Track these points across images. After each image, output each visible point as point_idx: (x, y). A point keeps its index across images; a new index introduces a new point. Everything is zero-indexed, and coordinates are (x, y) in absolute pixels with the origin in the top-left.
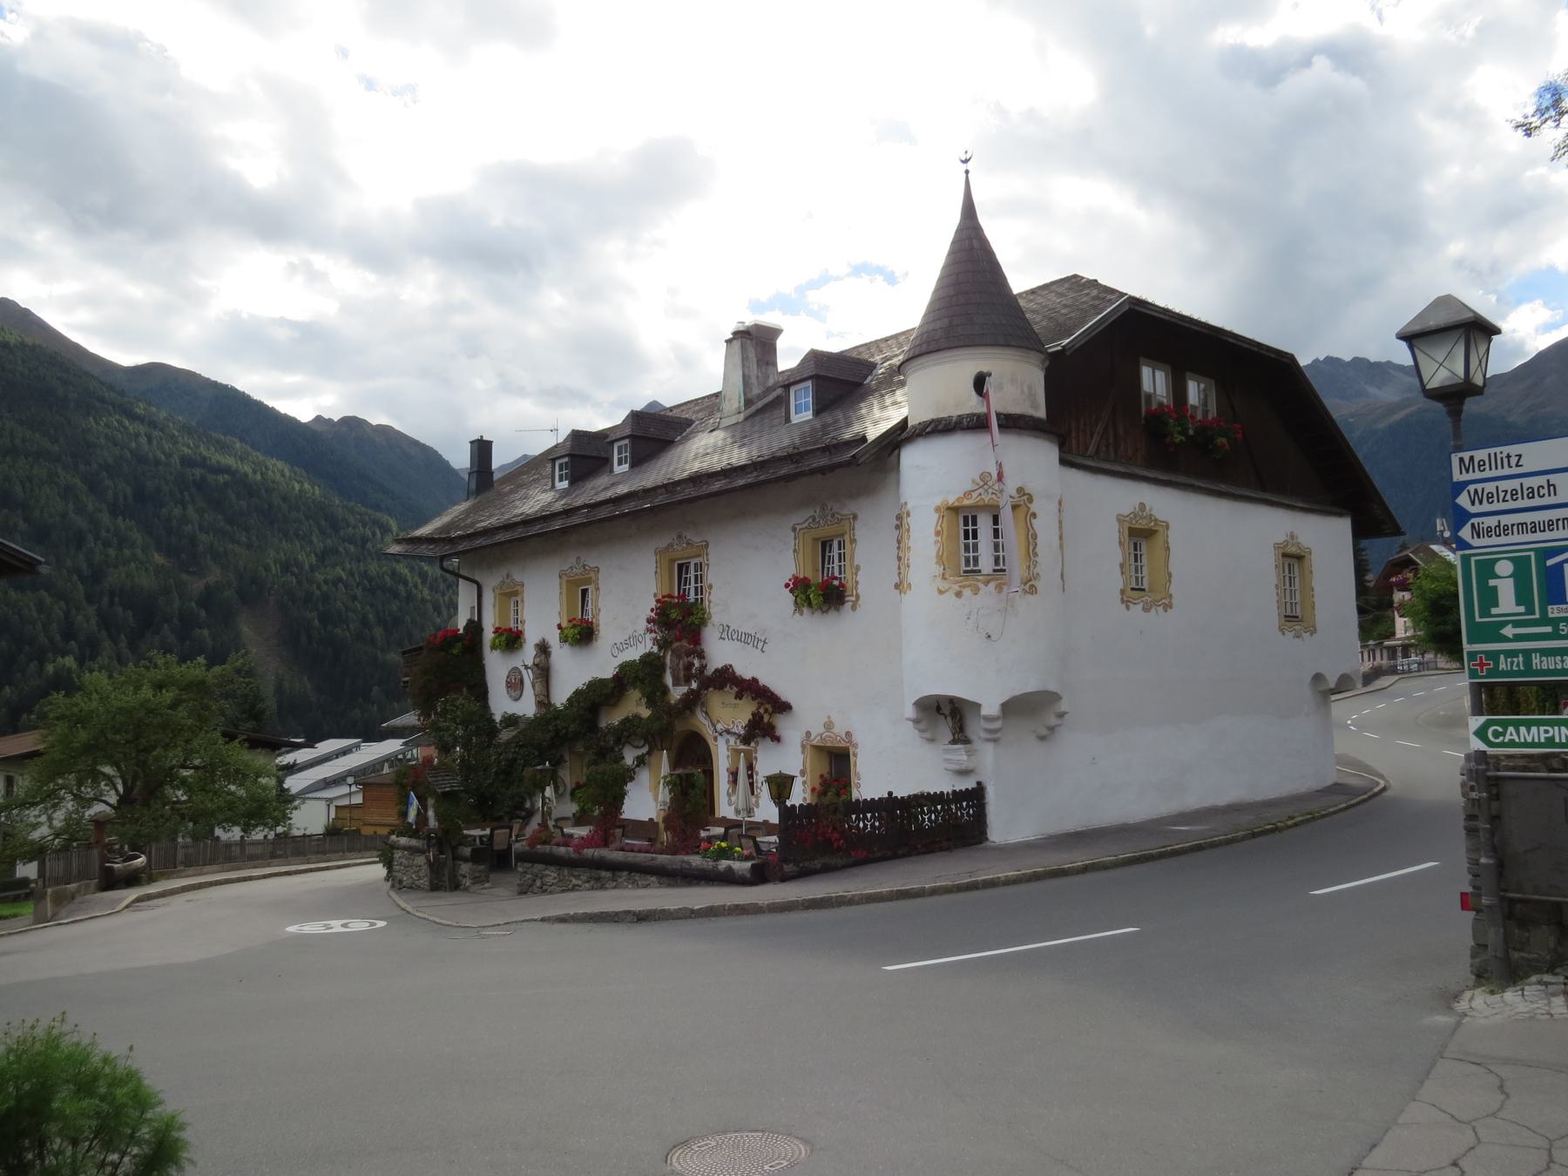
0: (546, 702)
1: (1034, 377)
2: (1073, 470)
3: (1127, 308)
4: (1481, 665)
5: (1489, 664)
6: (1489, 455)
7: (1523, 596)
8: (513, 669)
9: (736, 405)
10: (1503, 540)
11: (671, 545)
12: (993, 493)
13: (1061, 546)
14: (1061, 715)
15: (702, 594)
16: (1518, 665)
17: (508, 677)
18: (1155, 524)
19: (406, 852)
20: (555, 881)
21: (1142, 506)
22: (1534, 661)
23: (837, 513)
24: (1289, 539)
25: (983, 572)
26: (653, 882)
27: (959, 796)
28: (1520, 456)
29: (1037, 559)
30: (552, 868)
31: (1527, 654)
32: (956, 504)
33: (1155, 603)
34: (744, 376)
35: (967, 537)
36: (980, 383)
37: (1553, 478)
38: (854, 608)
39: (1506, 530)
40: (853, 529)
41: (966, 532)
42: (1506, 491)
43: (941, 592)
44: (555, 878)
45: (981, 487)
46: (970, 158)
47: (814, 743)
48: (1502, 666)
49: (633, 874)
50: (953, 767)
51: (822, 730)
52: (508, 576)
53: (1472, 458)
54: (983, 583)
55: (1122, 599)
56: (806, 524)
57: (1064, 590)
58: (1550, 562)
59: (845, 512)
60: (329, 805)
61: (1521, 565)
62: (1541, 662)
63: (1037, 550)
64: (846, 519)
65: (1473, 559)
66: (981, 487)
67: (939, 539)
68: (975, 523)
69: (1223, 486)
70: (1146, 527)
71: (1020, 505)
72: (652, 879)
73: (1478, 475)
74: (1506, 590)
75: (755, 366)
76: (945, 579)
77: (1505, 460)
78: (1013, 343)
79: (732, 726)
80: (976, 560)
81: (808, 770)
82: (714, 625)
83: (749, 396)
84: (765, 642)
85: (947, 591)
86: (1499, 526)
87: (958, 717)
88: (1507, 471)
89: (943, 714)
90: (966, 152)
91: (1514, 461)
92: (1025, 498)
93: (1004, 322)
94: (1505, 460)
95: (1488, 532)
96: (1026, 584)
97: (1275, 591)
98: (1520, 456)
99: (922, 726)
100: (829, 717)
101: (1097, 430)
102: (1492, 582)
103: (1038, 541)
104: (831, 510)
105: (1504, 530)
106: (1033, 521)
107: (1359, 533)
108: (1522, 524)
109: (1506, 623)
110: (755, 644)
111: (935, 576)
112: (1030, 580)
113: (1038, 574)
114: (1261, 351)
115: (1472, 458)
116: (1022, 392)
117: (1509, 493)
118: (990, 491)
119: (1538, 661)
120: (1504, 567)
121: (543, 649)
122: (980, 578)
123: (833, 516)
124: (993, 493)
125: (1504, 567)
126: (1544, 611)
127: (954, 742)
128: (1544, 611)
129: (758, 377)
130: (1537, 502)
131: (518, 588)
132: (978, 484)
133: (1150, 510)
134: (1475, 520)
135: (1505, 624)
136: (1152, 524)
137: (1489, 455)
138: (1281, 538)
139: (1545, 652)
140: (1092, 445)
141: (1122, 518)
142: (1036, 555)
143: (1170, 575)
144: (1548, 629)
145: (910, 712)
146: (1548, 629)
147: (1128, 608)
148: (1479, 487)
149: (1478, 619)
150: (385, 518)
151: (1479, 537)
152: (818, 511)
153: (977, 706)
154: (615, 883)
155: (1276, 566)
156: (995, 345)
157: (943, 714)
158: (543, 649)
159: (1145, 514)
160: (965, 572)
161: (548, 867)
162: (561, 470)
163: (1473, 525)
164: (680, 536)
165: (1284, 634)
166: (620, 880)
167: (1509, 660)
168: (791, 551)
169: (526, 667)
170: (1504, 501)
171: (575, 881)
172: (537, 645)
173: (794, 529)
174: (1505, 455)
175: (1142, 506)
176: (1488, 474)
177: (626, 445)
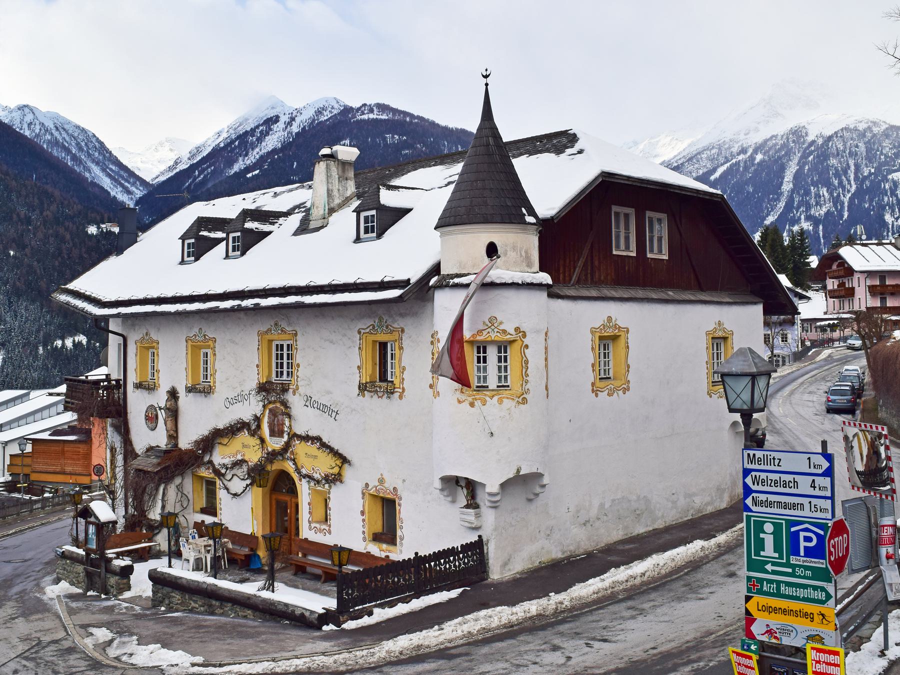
0: (175, 435)
1: (531, 242)
2: (560, 300)
3: (601, 180)
4: (754, 586)
5: (758, 586)
6: (764, 455)
7: (777, 548)
8: (150, 406)
9: (322, 212)
10: (768, 510)
11: (269, 330)
12: (497, 332)
13: (546, 366)
14: (544, 486)
15: (292, 369)
16: (773, 589)
17: (146, 412)
18: (619, 330)
19: (68, 561)
20: (179, 602)
21: (610, 319)
22: (782, 588)
23: (391, 326)
24: (717, 326)
25: (490, 388)
26: (249, 614)
27: (466, 548)
28: (780, 460)
29: (528, 378)
30: (177, 592)
31: (779, 583)
32: (472, 339)
33: (616, 389)
34: (328, 190)
35: (479, 362)
36: (492, 250)
37: (797, 478)
38: (401, 397)
39: (770, 504)
40: (402, 340)
41: (479, 358)
42: (772, 480)
43: (459, 402)
44: (179, 600)
45: (490, 327)
46: (489, 75)
47: (371, 492)
48: (765, 588)
49: (235, 606)
50: (467, 524)
51: (377, 484)
52: (147, 334)
53: (754, 455)
54: (489, 397)
55: (593, 390)
56: (368, 330)
57: (547, 397)
58: (793, 529)
59: (396, 325)
60: (4, 447)
61: (777, 527)
62: (785, 590)
63: (528, 372)
64: (396, 331)
65: (752, 518)
66: (490, 327)
67: (459, 363)
68: (485, 352)
69: (671, 293)
70: (612, 334)
71: (516, 340)
72: (248, 612)
73: (757, 467)
74: (769, 541)
75: (337, 181)
76: (463, 393)
77: (772, 460)
78: (515, 222)
79: (312, 472)
80: (485, 378)
81: (366, 511)
82: (300, 395)
83: (332, 205)
84: (337, 412)
85: (464, 401)
86: (767, 501)
87: (471, 488)
88: (772, 468)
89: (461, 486)
90: (486, 70)
91: (777, 462)
92: (520, 334)
93: (509, 204)
94: (772, 460)
95: (761, 503)
96: (519, 397)
97: (706, 366)
98: (780, 460)
99: (445, 493)
100: (382, 475)
101: (579, 265)
102: (762, 535)
103: (529, 365)
104: (386, 322)
105: (770, 504)
106: (526, 351)
107: (766, 312)
108: (779, 502)
109: (769, 562)
110: (330, 414)
111: (456, 390)
112: (523, 394)
113: (528, 389)
114: (699, 196)
115: (754, 455)
116: (521, 256)
117: (773, 482)
118: (496, 330)
119: (784, 589)
120: (769, 528)
121: (173, 394)
122: (487, 393)
123: (387, 327)
124: (497, 332)
125: (769, 528)
126: (788, 559)
127: (467, 506)
128: (788, 559)
129: (339, 190)
130: (787, 490)
131: (155, 344)
132: (487, 325)
133: (615, 321)
134: (754, 495)
135: (767, 562)
136: (617, 331)
137: (764, 455)
138: (711, 327)
139: (789, 584)
140: (575, 276)
141: (594, 330)
142: (527, 375)
143: (628, 367)
144: (790, 570)
145: (438, 484)
146: (790, 570)
147: (597, 395)
148: (758, 474)
149: (753, 557)
150: (50, 189)
151: (756, 506)
152: (377, 322)
153: (484, 485)
154: (222, 611)
155: (707, 348)
156: (503, 222)
157: (461, 486)
158: (173, 394)
159: (611, 324)
160: (477, 387)
161: (175, 591)
162: (189, 248)
163: (753, 497)
164: (276, 324)
165: (711, 397)
166: (226, 609)
167: (769, 585)
168: (357, 349)
169: (160, 409)
170: (770, 486)
171: (193, 604)
172: (168, 392)
173: (359, 332)
174: (772, 457)
175: (610, 319)
176: (762, 467)
177: (238, 237)
